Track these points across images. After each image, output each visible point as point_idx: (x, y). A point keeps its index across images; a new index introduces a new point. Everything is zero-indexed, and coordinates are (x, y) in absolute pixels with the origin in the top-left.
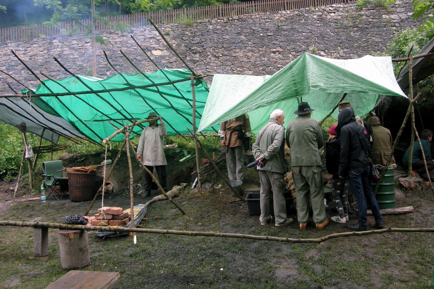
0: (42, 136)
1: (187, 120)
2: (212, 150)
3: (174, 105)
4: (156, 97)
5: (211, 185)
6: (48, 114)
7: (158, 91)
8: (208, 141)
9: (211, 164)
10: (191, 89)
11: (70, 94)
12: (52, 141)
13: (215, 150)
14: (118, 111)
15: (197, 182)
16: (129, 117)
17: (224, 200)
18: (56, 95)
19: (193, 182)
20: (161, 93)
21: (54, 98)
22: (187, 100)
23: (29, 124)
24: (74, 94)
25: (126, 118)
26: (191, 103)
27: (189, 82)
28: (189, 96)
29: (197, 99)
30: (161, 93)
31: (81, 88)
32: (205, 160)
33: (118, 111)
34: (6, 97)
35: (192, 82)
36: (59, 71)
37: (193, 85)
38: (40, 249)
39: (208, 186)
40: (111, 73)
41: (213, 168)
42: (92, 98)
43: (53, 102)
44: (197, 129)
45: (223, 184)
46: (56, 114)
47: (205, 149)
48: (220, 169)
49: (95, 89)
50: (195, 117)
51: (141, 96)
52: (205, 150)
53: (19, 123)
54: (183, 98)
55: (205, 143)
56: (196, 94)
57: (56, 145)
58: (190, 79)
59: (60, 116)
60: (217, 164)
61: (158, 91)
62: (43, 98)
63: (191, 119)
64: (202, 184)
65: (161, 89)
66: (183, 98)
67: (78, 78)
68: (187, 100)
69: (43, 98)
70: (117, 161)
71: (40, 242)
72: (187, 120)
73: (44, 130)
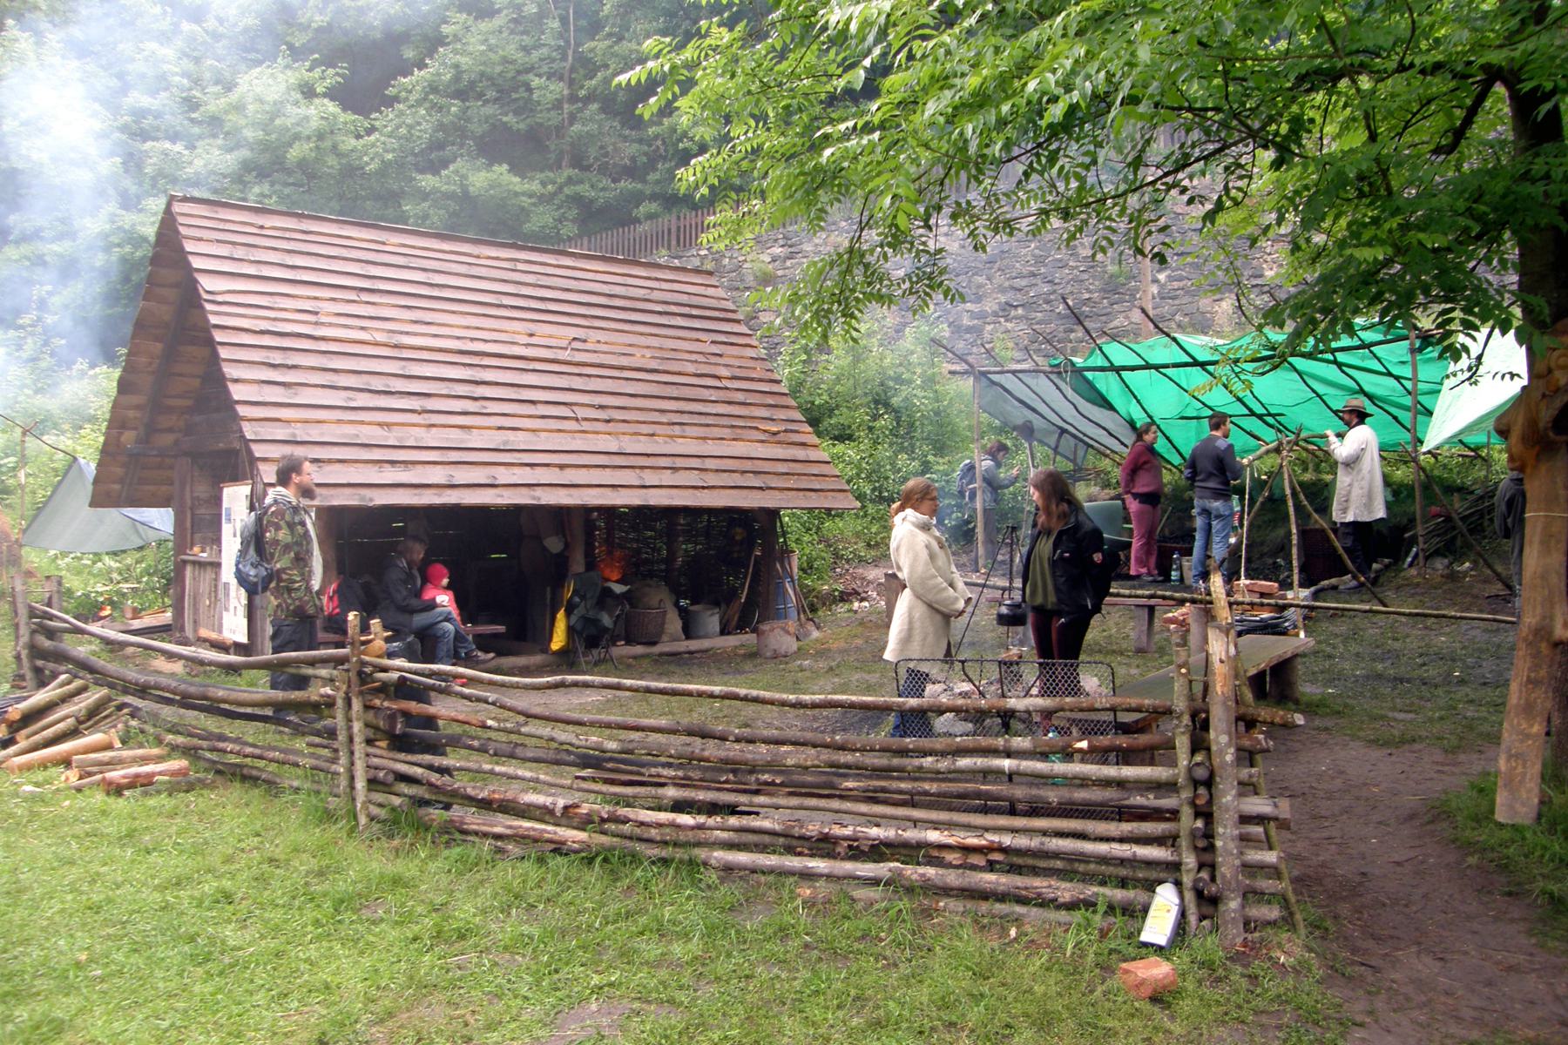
0: (1056, 450)
1: (1395, 418)
2: (1450, 489)
3: (1366, 388)
4: (1331, 372)
5: (1446, 561)
6: (1089, 405)
7: (1335, 362)
8: (1445, 466)
9: (1448, 519)
10: (1408, 358)
11: (1148, 366)
12: (1074, 461)
13: (1461, 490)
14: (1239, 400)
15: (1417, 555)
16: (1259, 410)
17: (1475, 591)
18: (1118, 370)
19: (1407, 555)
20: (1340, 365)
21: (1112, 376)
22: (1397, 378)
23: (1037, 422)
24: (1157, 367)
25: (1252, 413)
26: (1408, 385)
27: (1406, 343)
28: (1406, 371)
29: (1421, 376)
30: (1340, 365)
31: (1171, 354)
32: (1435, 509)
33: (1239, 400)
34: (1014, 372)
35: (1412, 344)
36: (1034, 275)
37: (1413, 351)
38: (1144, 638)
39: (1440, 564)
40: (1169, 277)
41: (1454, 528)
42: (1196, 377)
43: (1107, 384)
44: (1422, 443)
45: (1475, 562)
46: (1107, 405)
47: (1059, 124)
48: (1471, 531)
49: (1201, 358)
50: (1416, 413)
51: (1296, 370)
52: (1436, 488)
53: (1019, 422)
54: (1389, 374)
55: (1436, 473)
56: (1419, 368)
57: (1081, 469)
58: (1406, 338)
59: (1111, 408)
60: (1463, 519)
61: (1335, 362)
62: (1089, 375)
63: (1405, 417)
64: (1427, 558)
65: (1341, 357)
66: (1389, 374)
67: (1174, 339)
68: (1397, 378)
69: (1089, 375)
70: (1263, 504)
71: (1145, 628)
72: (1395, 418)
73: (1061, 435)
